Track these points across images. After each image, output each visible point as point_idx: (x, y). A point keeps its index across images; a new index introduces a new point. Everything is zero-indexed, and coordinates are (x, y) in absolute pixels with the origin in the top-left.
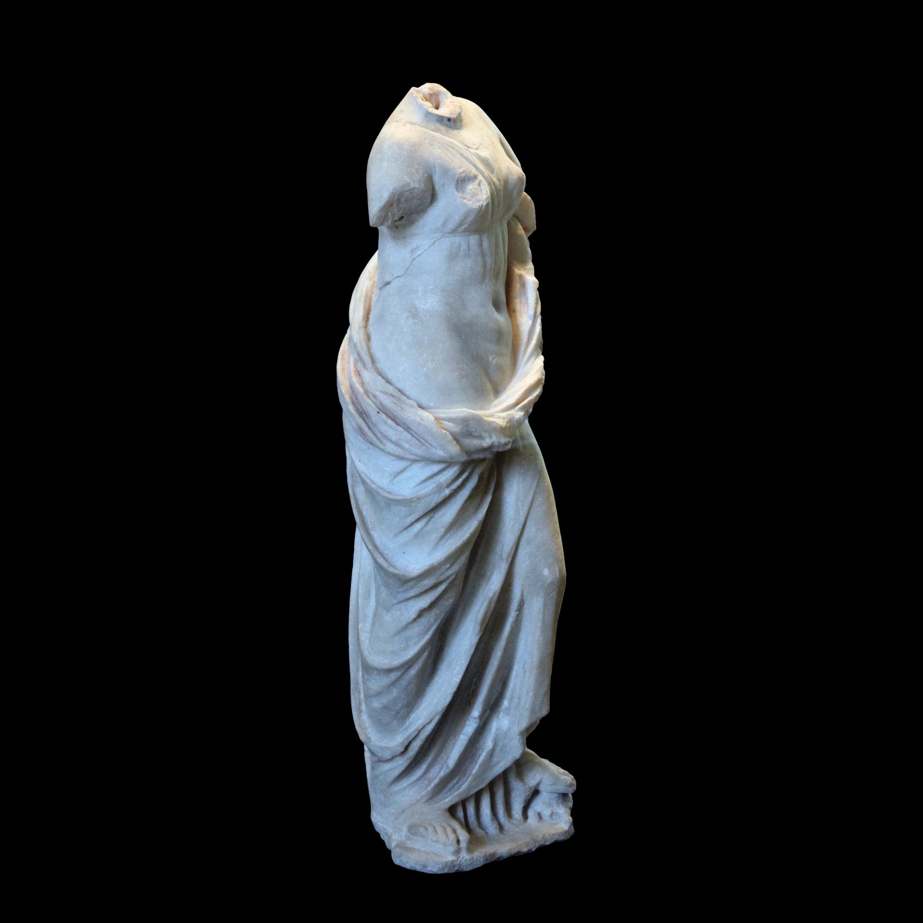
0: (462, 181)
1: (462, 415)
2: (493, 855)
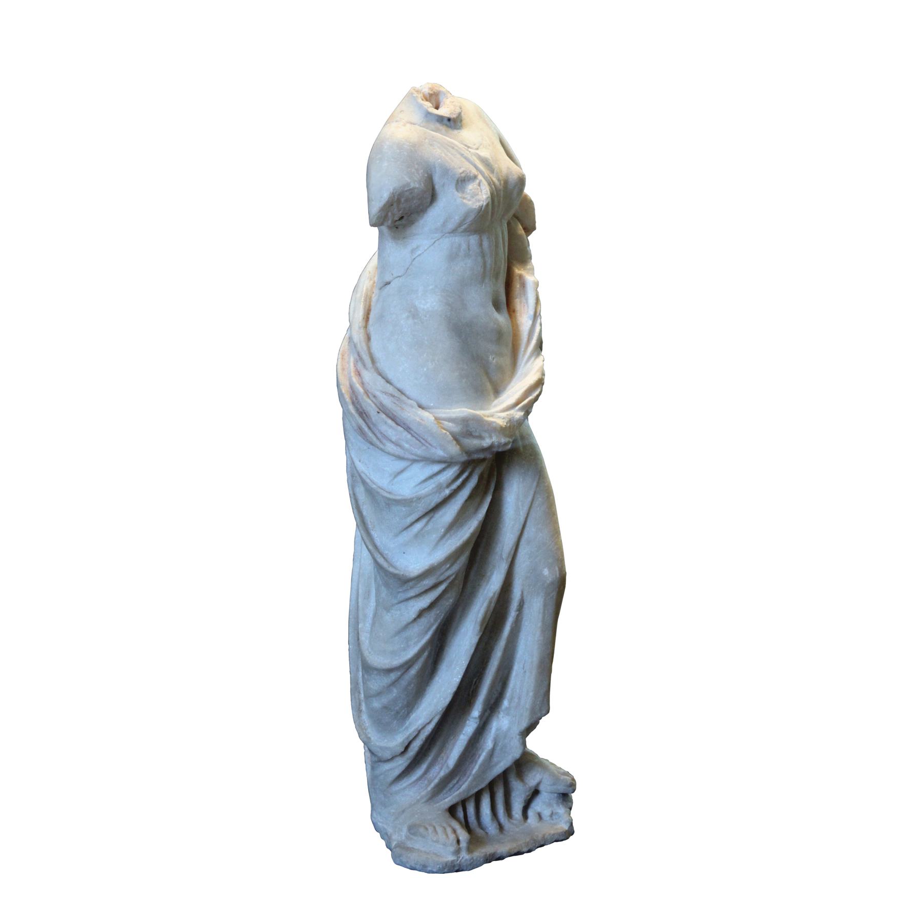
0: (462, 181)
1: (462, 415)
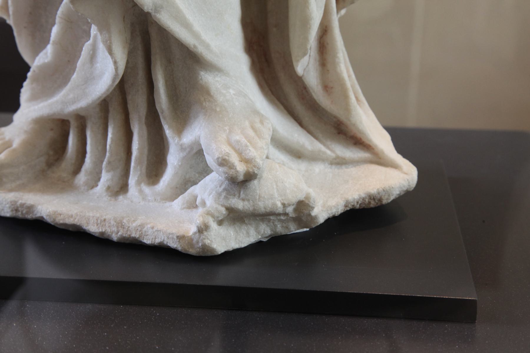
2: (30, 208)
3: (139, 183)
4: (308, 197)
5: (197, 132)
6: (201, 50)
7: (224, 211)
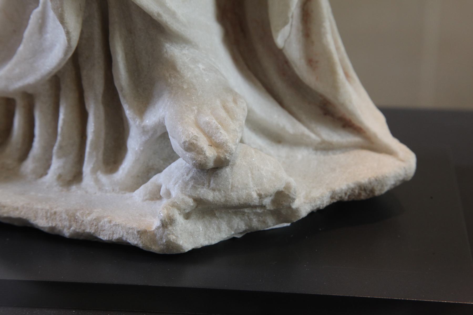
3: (94, 171)
4: (288, 187)
5: (162, 112)
6: (166, 18)
7: (191, 202)
